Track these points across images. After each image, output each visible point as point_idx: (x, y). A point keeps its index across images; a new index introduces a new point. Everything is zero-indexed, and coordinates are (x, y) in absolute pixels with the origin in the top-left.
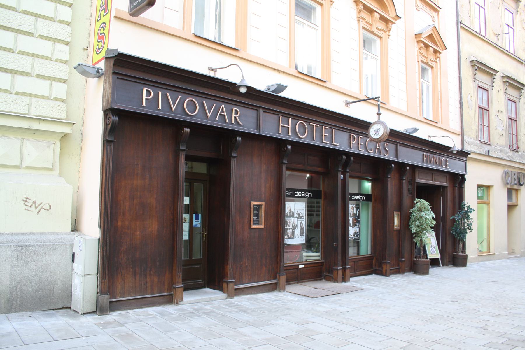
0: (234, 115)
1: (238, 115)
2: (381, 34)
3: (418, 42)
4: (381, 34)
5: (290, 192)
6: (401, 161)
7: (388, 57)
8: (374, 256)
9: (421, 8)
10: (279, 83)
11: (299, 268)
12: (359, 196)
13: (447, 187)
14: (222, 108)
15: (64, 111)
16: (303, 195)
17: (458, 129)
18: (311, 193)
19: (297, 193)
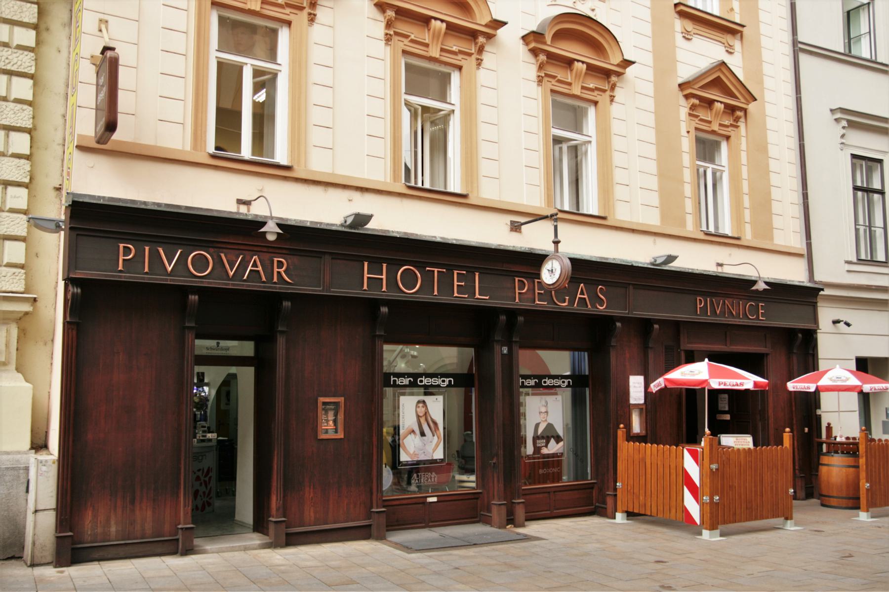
0: (276, 270)
1: (284, 269)
3: (687, 97)
4: (596, 96)
5: (534, 381)
6: (635, 314)
7: (612, 133)
9: (694, 34)
12: (405, 378)
13: (767, 354)
14: (255, 261)
15: (21, 280)
16: (434, 383)
17: (797, 243)
19: (423, 379)
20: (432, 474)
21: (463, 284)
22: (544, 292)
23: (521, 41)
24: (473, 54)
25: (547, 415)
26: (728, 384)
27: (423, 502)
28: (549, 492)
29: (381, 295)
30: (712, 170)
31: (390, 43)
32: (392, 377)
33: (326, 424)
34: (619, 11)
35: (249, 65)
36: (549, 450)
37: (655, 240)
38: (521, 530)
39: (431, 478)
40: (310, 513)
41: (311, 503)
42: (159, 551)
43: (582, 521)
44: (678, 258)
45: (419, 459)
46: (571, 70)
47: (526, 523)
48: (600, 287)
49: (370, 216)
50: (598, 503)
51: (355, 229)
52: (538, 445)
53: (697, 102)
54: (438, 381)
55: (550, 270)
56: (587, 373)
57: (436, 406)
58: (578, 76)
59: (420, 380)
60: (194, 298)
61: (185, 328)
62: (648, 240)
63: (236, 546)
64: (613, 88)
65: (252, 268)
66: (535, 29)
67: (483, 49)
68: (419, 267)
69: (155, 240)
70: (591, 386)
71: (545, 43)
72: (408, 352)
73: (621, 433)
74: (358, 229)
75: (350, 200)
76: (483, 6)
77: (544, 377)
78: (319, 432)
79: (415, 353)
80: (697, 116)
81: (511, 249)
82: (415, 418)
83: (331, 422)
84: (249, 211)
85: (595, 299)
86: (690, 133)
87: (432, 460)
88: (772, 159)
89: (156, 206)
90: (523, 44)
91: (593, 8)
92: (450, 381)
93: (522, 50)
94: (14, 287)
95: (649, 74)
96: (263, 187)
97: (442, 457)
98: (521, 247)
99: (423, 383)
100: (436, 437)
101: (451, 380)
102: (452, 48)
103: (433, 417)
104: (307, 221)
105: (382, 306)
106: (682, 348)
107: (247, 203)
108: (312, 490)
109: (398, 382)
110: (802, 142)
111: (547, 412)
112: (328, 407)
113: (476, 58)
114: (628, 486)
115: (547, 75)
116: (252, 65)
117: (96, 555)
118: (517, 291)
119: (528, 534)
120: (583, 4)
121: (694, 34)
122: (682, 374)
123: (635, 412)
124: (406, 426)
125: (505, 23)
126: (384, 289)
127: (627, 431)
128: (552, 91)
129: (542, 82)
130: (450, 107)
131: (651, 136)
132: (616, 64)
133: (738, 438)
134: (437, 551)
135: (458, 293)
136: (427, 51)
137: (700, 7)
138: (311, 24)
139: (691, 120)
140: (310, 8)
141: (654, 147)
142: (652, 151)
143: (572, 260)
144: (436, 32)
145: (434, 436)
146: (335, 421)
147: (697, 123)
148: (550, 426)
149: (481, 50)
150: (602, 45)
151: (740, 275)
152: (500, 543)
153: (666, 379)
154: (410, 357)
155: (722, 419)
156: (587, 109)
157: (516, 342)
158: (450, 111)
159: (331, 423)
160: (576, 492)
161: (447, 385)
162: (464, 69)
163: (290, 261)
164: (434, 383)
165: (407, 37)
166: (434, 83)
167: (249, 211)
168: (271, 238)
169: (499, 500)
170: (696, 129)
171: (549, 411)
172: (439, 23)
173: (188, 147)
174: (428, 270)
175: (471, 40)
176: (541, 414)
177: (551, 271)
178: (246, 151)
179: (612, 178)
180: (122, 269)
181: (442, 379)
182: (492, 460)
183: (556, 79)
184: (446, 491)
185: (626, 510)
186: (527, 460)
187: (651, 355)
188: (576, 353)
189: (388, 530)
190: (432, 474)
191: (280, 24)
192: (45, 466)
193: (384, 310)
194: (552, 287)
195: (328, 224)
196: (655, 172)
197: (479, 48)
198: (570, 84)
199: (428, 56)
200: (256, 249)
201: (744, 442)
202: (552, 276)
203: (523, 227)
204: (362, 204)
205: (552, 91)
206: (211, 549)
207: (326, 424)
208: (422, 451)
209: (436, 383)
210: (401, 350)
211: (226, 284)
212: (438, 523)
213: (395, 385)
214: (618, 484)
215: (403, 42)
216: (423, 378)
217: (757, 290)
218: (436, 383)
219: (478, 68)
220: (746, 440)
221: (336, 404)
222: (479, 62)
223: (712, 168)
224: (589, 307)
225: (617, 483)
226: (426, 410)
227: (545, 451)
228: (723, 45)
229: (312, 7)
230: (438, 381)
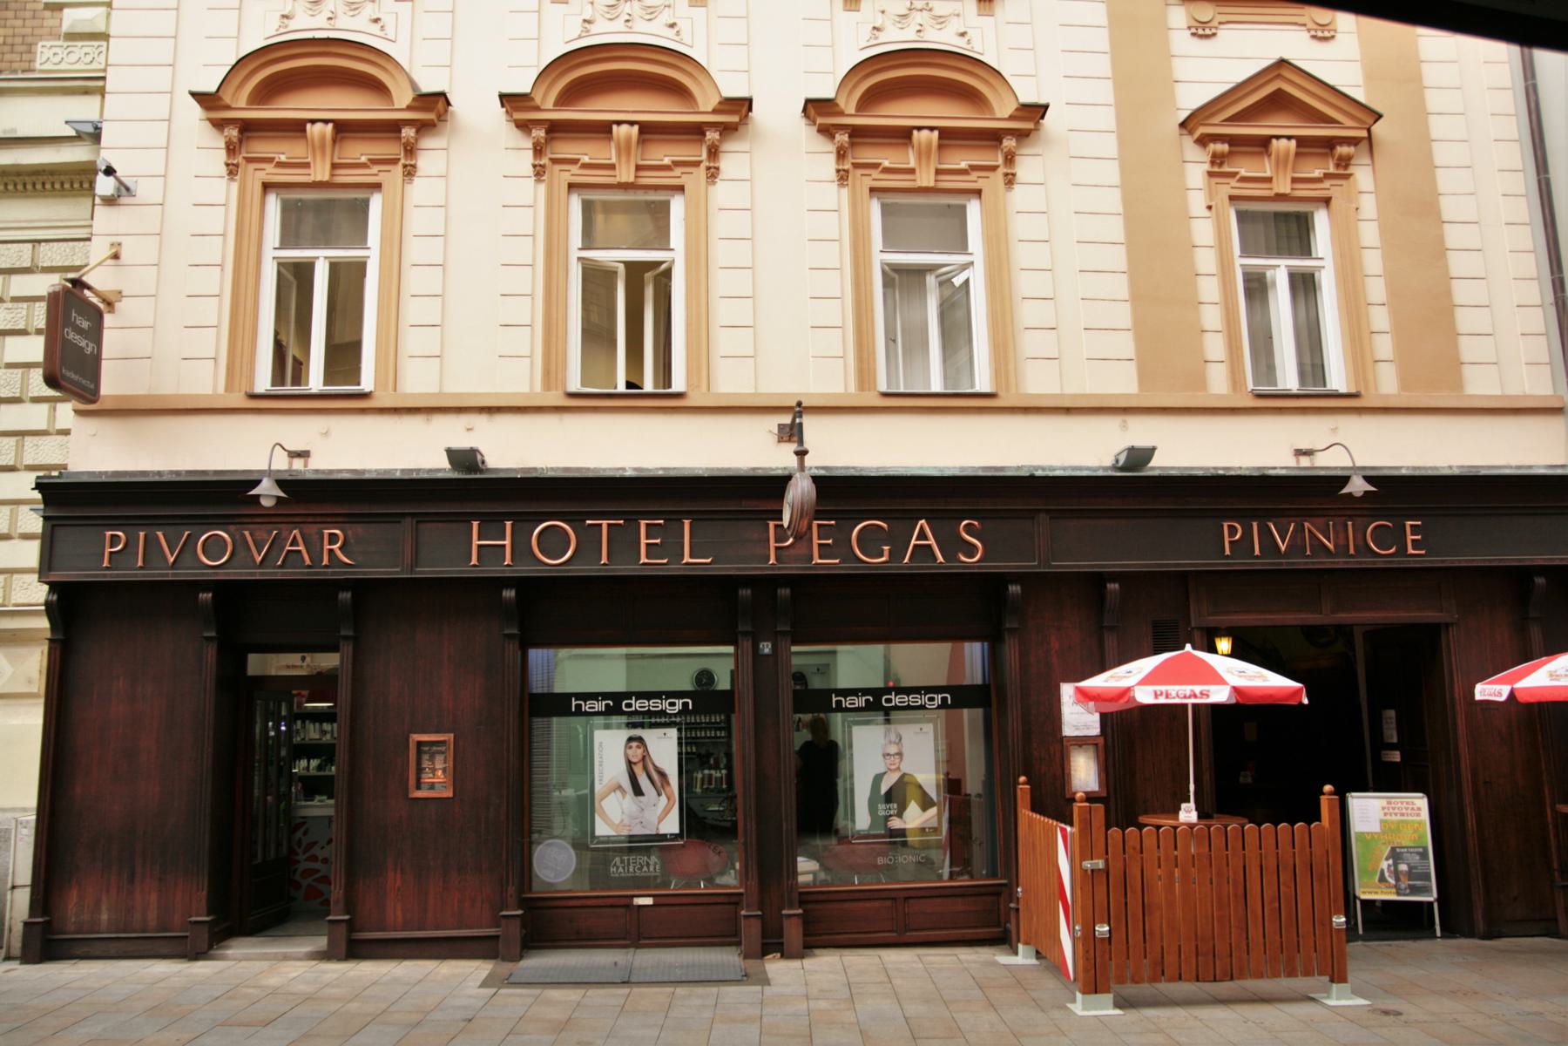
3: (1203, 141)
4: (975, 182)
8: (741, 894)
9: (1220, 23)
10: (1130, 444)
14: (1310, 531)
18: (949, 693)
20: (649, 858)
24: (701, 162)
25: (901, 759)
26: (1174, 694)
28: (894, 899)
29: (503, 571)
30: (1243, 269)
31: (543, 178)
35: (322, 259)
36: (905, 822)
39: (648, 865)
40: (395, 910)
42: (165, 951)
44: (1156, 452)
53: (1225, 148)
54: (922, 700)
57: (664, 747)
58: (923, 154)
62: (1111, 424)
63: (271, 953)
65: (919, 542)
69: (1263, 515)
74: (1138, 471)
75: (468, 430)
76: (705, 82)
77: (887, 690)
82: (623, 767)
84: (306, 465)
85: (953, 545)
87: (657, 835)
88: (1365, 222)
90: (806, 125)
93: (803, 133)
94: (20, 597)
96: (328, 429)
99: (633, 709)
100: (663, 798)
101: (688, 703)
102: (662, 160)
104: (397, 470)
107: (1308, 453)
108: (399, 876)
110: (1542, 176)
111: (900, 754)
112: (435, 748)
116: (326, 258)
117: (79, 951)
118: (772, 544)
121: (1220, 23)
124: (606, 780)
125: (194, 95)
132: (1006, 116)
133: (1393, 800)
134: (529, 988)
144: (923, 146)
145: (659, 794)
150: (973, 88)
151: (996, 469)
152: (595, 985)
155: (1389, 760)
156: (1312, 213)
159: (440, 773)
160: (960, 899)
163: (349, 533)
165: (574, 162)
167: (306, 465)
168: (266, 503)
171: (905, 751)
172: (1284, 142)
173: (852, 389)
174: (590, 525)
175: (1325, 155)
178: (316, 380)
181: (927, 696)
183: (880, 169)
190: (649, 858)
192: (25, 827)
195: (430, 471)
200: (296, 520)
201: (1407, 809)
204: (1140, 433)
206: (233, 954)
207: (431, 775)
208: (637, 821)
211: (251, 574)
216: (631, 699)
217: (1350, 495)
218: (658, 707)
220: (1413, 804)
223: (1286, 266)
228: (1303, 28)
230: (662, 704)
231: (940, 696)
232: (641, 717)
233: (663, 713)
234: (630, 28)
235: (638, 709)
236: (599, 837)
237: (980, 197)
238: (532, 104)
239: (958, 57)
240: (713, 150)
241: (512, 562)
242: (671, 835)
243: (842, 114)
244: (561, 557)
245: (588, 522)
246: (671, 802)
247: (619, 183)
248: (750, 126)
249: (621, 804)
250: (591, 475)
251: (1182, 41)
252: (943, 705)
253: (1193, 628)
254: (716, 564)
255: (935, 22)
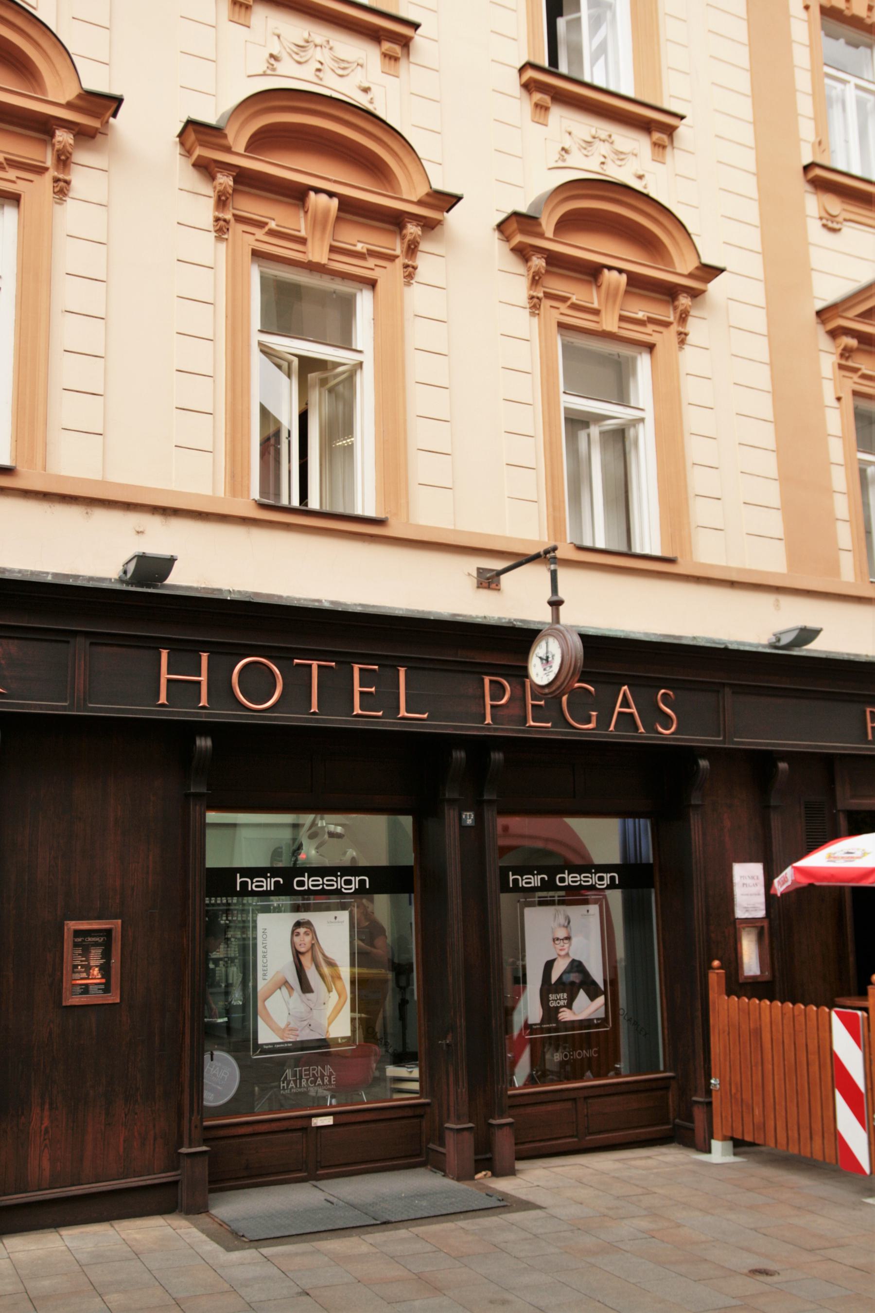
2: (650, 335)
3: (834, 334)
4: (650, 335)
5: (539, 877)
9: (845, 220)
11: (313, 1125)
12: (533, 875)
16: (585, 881)
18: (294, 879)
19: (306, 879)
21: (373, 689)
22: (545, 702)
23: (497, 234)
24: (397, 257)
27: (303, 1127)
28: (574, 1099)
31: (225, 236)
32: (238, 875)
33: (84, 975)
34: (692, 180)
36: (574, 1013)
37: (777, 600)
38: (503, 1185)
41: (45, 1140)
43: (641, 1158)
45: (298, 1039)
46: (599, 287)
47: (519, 1165)
48: (663, 691)
49: (169, 559)
50: (680, 1119)
51: (148, 586)
52: (553, 1004)
53: (853, 342)
54: (338, 883)
55: (545, 658)
56: (651, 861)
59: (560, 878)
60: (204, 743)
61: (188, 796)
64: (683, 318)
66: (523, 209)
67: (416, 247)
68: (281, 658)
70: (658, 884)
71: (541, 236)
72: (323, 828)
73: (716, 977)
75: (138, 532)
78: (66, 993)
79: (339, 829)
80: (855, 370)
81: (479, 620)
82: (289, 957)
83: (97, 969)
86: (843, 400)
89: (125, 585)
90: (499, 239)
91: (641, 173)
92: (362, 882)
95: (757, 293)
97: (348, 1033)
98: (499, 618)
100: (334, 995)
101: (365, 880)
103: (327, 954)
105: (780, 762)
106: (840, 805)
108: (46, 1113)
109: (522, 883)
113: (677, 332)
114: (730, 1084)
115: (548, 296)
118: (488, 702)
119: (513, 1193)
120: (620, 166)
121: (845, 220)
122: (830, 857)
123: (748, 934)
124: (271, 974)
126: (204, 702)
127: (726, 973)
128: (561, 326)
129: (539, 309)
130: (357, 357)
131: (764, 406)
135: (362, 708)
136: (304, 253)
137: (856, 171)
138: (61, 199)
139: (844, 376)
140: (57, 169)
141: (771, 427)
142: (766, 435)
143: (586, 639)
145: (330, 991)
146: (105, 969)
147: (855, 383)
148: (577, 966)
149: (412, 249)
153: (798, 870)
154: (326, 836)
156: (355, 295)
157: (490, 802)
158: (355, 365)
159: (96, 972)
161: (607, 885)
162: (379, 286)
164: (585, 881)
165: (261, 225)
166: (333, 316)
169: (459, 1120)
170: (855, 393)
171: (572, 935)
172: (323, 198)
174: (298, 665)
176: (557, 942)
177: (546, 660)
179: (686, 486)
180: (166, 702)
182: (445, 1038)
183: (569, 303)
184: (363, 1103)
185: (729, 1134)
186: (527, 1035)
187: (776, 822)
188: (630, 822)
189: (212, 1191)
191: (360, 286)
193: (204, 743)
194: (547, 691)
196: (774, 474)
197: (409, 246)
198: (596, 312)
199: (600, 329)
202: (548, 669)
203: (503, 577)
205: (561, 326)
208: (305, 1023)
209: (333, 885)
210: (313, 824)
212: (363, 1167)
213: (517, 888)
214: (713, 1081)
215: (253, 234)
219: (408, 284)
221: (108, 933)
222: (410, 272)
224: (642, 730)
225: (710, 1078)
226: (313, 939)
227: (566, 1015)
229: (681, 323)
230: (337, 882)
231: (357, 879)
232: (300, 897)
233: (338, 892)
234: (321, 79)
235: (254, 889)
236: (262, 1045)
237: (18, 206)
238: (222, 141)
239: (656, 205)
240: (413, 247)
241: (167, 700)
242: (343, 1038)
243: (228, 150)
244: (573, 719)
245: (296, 661)
246: (342, 1000)
247: (310, 262)
248: (445, 226)
249: (287, 1003)
250: (284, 603)
251: (815, 230)
252: (361, 890)
253: (839, 811)
254: (679, 734)
255: (616, 157)
